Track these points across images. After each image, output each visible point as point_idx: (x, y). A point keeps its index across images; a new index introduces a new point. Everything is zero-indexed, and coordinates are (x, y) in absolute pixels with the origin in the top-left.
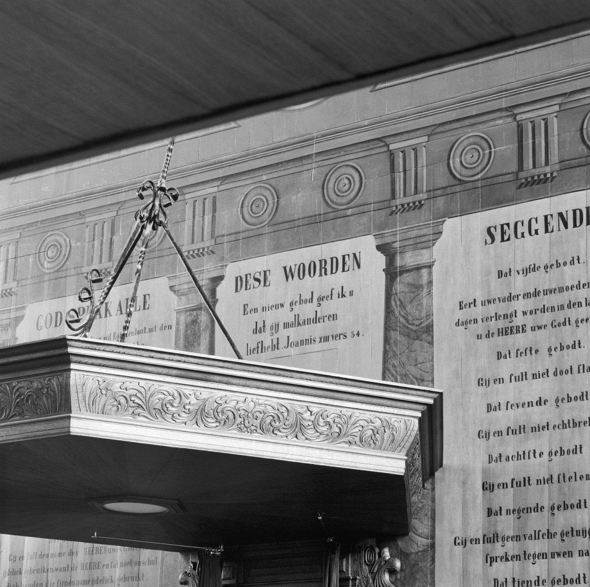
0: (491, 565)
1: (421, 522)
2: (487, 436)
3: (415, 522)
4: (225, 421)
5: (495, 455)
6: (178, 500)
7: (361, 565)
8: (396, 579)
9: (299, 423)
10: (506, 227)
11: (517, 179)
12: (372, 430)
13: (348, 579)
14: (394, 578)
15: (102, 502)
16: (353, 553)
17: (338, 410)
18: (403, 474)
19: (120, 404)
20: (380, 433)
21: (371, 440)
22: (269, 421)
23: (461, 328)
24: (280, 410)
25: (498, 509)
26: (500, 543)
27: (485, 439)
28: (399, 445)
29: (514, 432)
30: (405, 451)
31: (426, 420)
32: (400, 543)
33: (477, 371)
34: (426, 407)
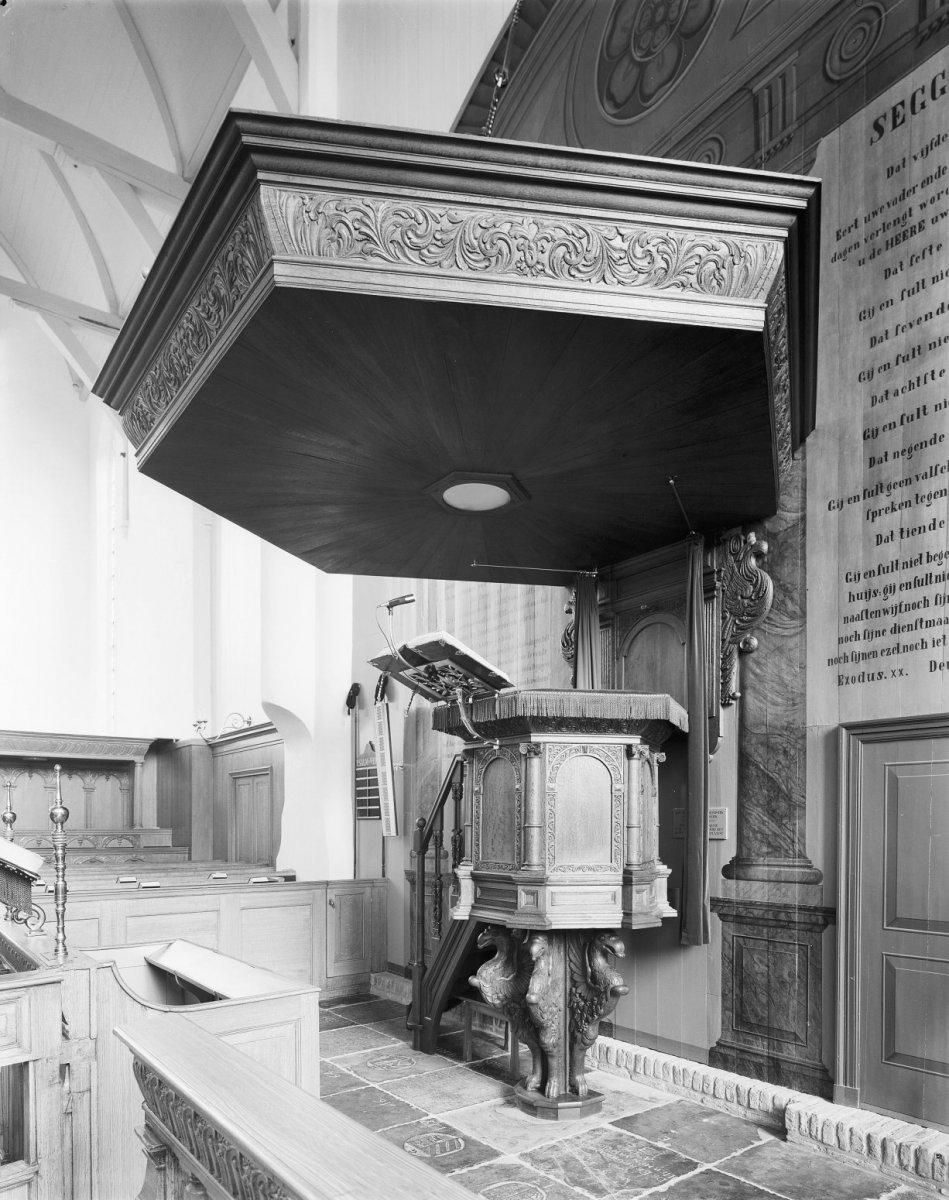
0: (873, 521)
1: (791, 496)
2: (870, 375)
3: (783, 499)
4: (498, 258)
5: (880, 394)
6: (509, 474)
7: (726, 556)
8: (764, 562)
9: (605, 256)
10: (899, 108)
11: (918, 34)
12: (715, 261)
13: (713, 572)
14: (760, 562)
15: (437, 491)
16: (719, 544)
17: (662, 232)
18: (761, 330)
19: (340, 236)
20: (726, 266)
21: (713, 281)
22: (562, 255)
23: (839, 262)
24: (576, 234)
25: (882, 455)
26: (886, 492)
27: (867, 380)
28: (756, 286)
29: (906, 359)
30: (764, 295)
31: (796, 240)
32: (768, 525)
33: (858, 304)
34: (794, 218)
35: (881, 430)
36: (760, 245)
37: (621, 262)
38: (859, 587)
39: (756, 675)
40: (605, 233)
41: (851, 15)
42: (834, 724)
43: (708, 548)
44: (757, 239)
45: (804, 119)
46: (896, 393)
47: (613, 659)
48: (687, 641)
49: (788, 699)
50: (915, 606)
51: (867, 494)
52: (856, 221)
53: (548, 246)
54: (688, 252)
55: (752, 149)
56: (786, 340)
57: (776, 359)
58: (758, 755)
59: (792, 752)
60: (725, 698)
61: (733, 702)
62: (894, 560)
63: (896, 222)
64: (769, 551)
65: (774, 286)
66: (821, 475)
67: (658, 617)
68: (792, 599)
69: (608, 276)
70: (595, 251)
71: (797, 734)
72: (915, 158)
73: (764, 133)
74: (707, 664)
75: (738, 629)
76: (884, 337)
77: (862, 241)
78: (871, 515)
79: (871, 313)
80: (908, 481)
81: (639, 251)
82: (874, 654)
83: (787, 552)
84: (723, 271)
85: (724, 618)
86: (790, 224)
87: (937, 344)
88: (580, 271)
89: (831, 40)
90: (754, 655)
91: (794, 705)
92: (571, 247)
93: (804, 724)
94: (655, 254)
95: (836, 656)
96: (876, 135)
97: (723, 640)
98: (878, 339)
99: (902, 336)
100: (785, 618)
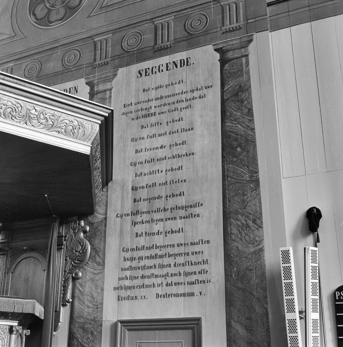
0: (134, 226)
2: (135, 165)
3: (97, 208)
5: (139, 173)
7: (69, 229)
8: (87, 235)
9: (28, 115)
10: (147, 70)
11: (154, 48)
12: (72, 126)
13: (63, 236)
16: (66, 223)
17: (52, 112)
18: (89, 154)
20: (76, 129)
21: (71, 133)
22: (9, 111)
25: (139, 199)
26: (140, 215)
29: (149, 162)
30: (90, 142)
32: (90, 218)
33: (132, 135)
34: (103, 118)
35: (138, 188)
36: (90, 124)
37: (34, 119)
38: (128, 255)
39: (80, 291)
40: (29, 107)
41: (132, 32)
42: (115, 320)
43: (61, 224)
44: (89, 122)
45: (113, 58)
46: (145, 175)
47: (5, 273)
48: (46, 268)
49: (95, 305)
50: (151, 267)
51: (133, 214)
52: (131, 103)
53: (4, 107)
54: (62, 121)
55: (93, 61)
56: (99, 153)
57: (95, 160)
58: (79, 333)
59: (95, 333)
60: (64, 301)
61: (68, 304)
62: (143, 245)
63: (146, 109)
64: (90, 231)
65: (96, 136)
66: (115, 201)
67: (33, 254)
68: (99, 255)
69: (28, 123)
70: (24, 113)
71: (98, 323)
72: (153, 89)
73: (98, 56)
74: (56, 283)
75: (72, 266)
76: (141, 151)
77: (133, 112)
78: (134, 224)
79: (136, 140)
80: (149, 212)
81: (42, 117)
82: (134, 287)
83: (97, 233)
84: (75, 130)
85: (66, 260)
86: (102, 119)
87: (160, 160)
88: (16, 118)
89: (124, 36)
90: (80, 281)
91: (97, 308)
92: (14, 109)
93: (102, 319)
94: (48, 119)
95: (117, 286)
96: (139, 76)
97: (65, 271)
98: (138, 151)
99: (147, 153)
100: (95, 265)
